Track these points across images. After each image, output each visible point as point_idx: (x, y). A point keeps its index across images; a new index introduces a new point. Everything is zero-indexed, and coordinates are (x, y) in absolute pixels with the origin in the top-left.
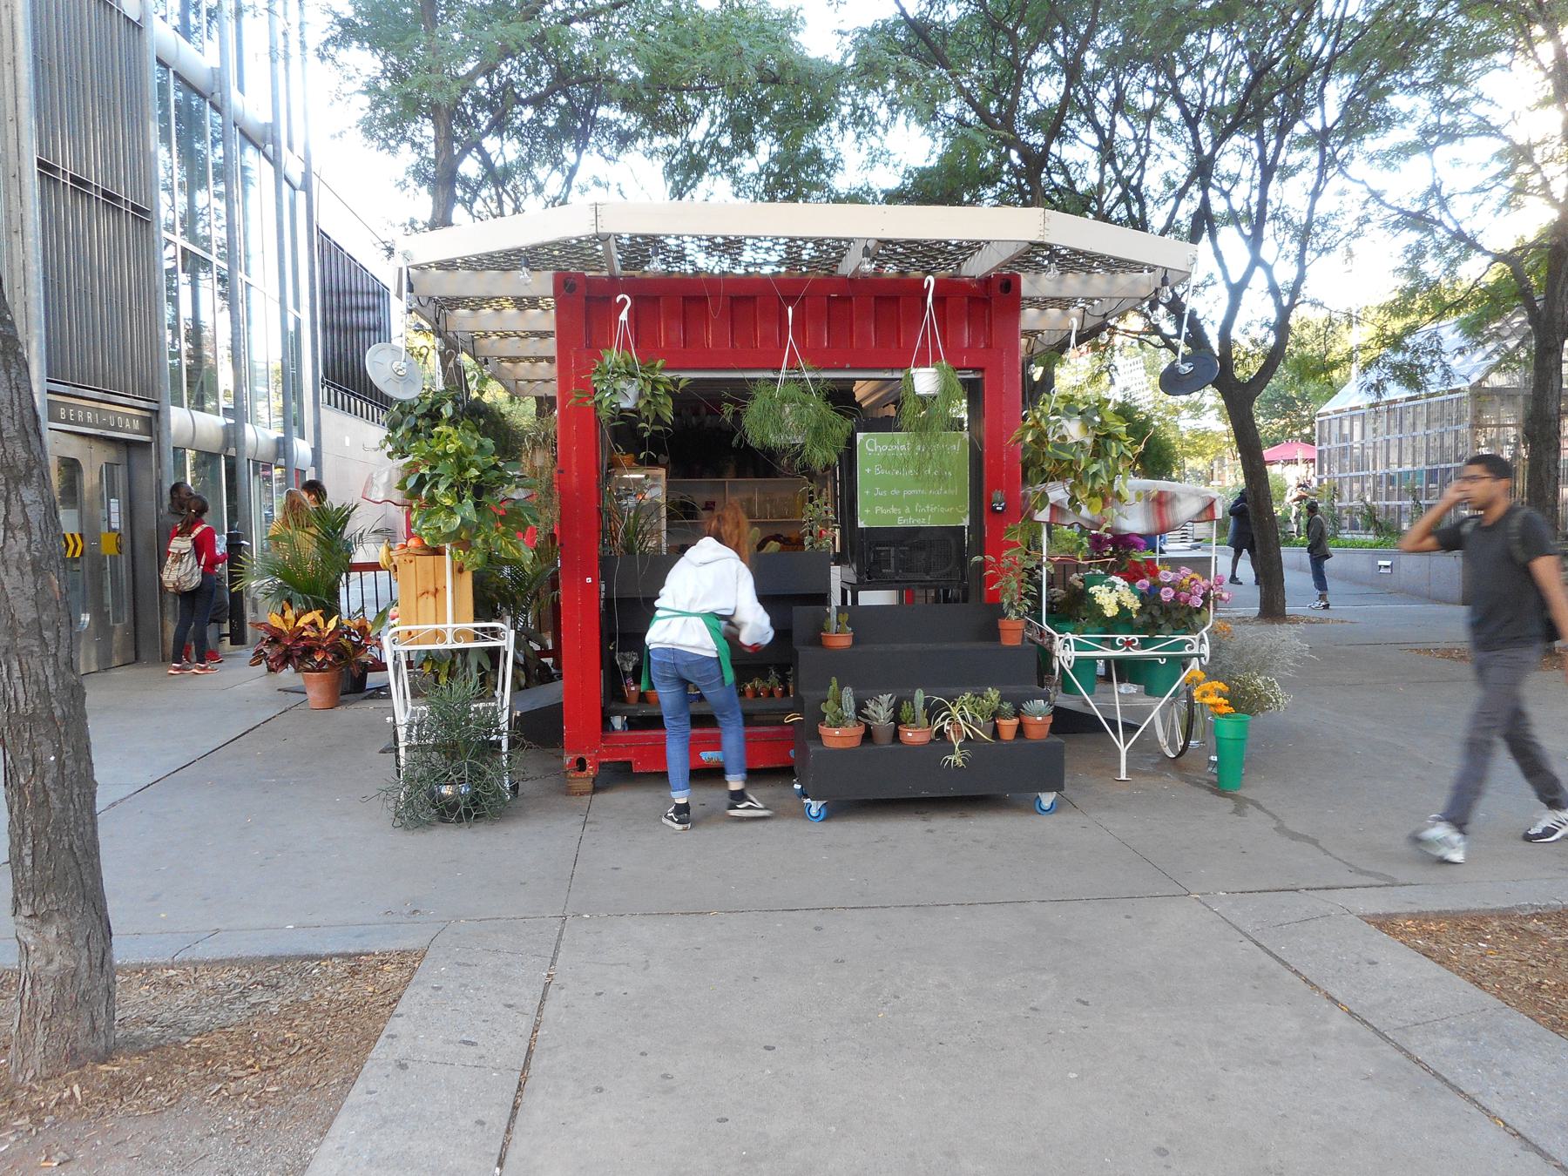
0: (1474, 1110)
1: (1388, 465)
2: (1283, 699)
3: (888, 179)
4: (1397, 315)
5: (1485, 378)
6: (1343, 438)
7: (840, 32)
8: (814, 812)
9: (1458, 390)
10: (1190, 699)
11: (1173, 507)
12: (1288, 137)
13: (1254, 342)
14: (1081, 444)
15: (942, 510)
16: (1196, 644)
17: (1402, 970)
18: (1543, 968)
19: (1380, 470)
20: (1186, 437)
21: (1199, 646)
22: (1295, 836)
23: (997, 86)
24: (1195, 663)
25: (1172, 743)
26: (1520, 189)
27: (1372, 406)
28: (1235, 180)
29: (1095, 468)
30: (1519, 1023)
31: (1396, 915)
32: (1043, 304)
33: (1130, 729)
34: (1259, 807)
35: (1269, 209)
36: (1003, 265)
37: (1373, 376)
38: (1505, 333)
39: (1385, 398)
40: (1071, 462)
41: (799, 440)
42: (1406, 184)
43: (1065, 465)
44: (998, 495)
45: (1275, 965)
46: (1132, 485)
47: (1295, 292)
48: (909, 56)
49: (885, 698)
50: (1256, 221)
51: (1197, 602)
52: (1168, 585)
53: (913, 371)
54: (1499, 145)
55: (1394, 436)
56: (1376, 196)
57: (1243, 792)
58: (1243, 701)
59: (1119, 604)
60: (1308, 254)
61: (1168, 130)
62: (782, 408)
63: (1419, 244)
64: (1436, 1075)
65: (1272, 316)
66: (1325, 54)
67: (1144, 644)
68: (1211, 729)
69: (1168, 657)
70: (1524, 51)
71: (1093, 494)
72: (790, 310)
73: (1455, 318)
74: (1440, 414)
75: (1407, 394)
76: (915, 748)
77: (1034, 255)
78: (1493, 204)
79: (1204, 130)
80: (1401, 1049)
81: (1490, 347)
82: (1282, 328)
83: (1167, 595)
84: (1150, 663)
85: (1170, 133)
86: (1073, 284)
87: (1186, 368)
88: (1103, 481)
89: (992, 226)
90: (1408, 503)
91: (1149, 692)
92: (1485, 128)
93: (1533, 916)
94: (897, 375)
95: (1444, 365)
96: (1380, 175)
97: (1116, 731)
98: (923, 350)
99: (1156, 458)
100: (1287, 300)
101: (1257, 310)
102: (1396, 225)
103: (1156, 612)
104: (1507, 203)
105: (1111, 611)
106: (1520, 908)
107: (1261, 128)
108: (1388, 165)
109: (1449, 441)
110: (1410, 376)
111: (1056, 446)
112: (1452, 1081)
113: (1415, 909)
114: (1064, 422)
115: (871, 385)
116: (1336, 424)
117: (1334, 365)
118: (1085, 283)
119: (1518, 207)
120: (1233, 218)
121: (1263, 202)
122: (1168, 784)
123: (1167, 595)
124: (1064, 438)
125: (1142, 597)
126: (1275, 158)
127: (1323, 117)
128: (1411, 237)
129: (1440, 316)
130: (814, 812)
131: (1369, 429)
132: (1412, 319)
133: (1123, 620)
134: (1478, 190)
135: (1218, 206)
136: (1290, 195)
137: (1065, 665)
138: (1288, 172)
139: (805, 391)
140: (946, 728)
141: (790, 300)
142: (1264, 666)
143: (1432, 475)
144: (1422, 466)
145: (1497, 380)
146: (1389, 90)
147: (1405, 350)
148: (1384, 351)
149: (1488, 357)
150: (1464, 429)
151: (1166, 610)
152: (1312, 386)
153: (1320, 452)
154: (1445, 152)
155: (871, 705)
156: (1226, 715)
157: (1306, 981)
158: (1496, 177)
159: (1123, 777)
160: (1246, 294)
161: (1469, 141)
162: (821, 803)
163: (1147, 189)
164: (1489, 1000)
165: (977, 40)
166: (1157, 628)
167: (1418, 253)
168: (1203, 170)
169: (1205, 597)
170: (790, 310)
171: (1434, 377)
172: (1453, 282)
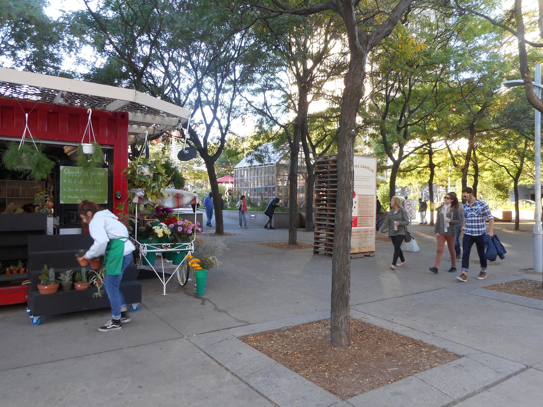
0: (267, 401)
1: (254, 185)
2: (218, 263)
3: (85, 70)
4: (256, 140)
5: (280, 161)
6: (241, 176)
7: (62, 11)
8: (35, 321)
9: (272, 164)
10: (188, 265)
11: (182, 199)
12: (225, 80)
13: (215, 144)
14: (149, 176)
15: (97, 197)
16: (190, 246)
17: (249, 353)
18: (289, 347)
19: (252, 187)
20: (196, 172)
21: (191, 247)
22: (220, 311)
23: (127, 44)
24: (189, 252)
25: (182, 280)
26: (288, 107)
27: (250, 167)
28: (209, 91)
29: (153, 185)
30: (281, 368)
31: (248, 335)
32: (139, 124)
33: (167, 275)
34: (210, 301)
35: (219, 102)
36: (119, 109)
37: (249, 158)
38: (285, 148)
39: (253, 165)
40: (145, 182)
41: (29, 168)
42: (258, 100)
43: (143, 183)
44: (118, 193)
45: (210, 359)
46: (171, 190)
47: (227, 129)
48: (88, 24)
49: (69, 272)
50: (216, 104)
51: (190, 232)
52: (181, 226)
53: (82, 144)
54: (283, 93)
55: (256, 177)
56: (250, 103)
57: (204, 296)
58: (205, 265)
59: (163, 232)
60: (231, 118)
61: (188, 70)
62: (21, 155)
63: (262, 119)
64: (257, 391)
65: (220, 136)
66: (236, 56)
67: (172, 247)
68: (195, 275)
69: (180, 251)
70: (289, 67)
71: (153, 194)
72: (27, 115)
73: (272, 143)
74: (268, 171)
75: (259, 164)
76: (81, 292)
77: (134, 106)
78: (281, 110)
79: (199, 73)
80: (247, 383)
81: (281, 152)
82: (222, 140)
83: (180, 229)
84: (174, 253)
85: (189, 73)
86: (149, 118)
87: (186, 152)
88: (156, 190)
89: (121, 94)
90: (260, 197)
91: (174, 263)
92: (280, 88)
93: (287, 330)
94: (77, 145)
95: (269, 156)
96: (250, 96)
97: (162, 277)
98: (87, 137)
99: (178, 181)
100: (224, 130)
101: (215, 133)
102: (255, 113)
103: (176, 235)
104: (285, 110)
105: (160, 235)
106: (283, 328)
107: (217, 77)
108: (254, 94)
109: (270, 179)
110: (260, 158)
111: (139, 175)
112: (261, 392)
113: (254, 332)
114: (143, 167)
115: (69, 148)
116: (239, 172)
117: (239, 153)
118: (153, 118)
119: (288, 112)
120: (208, 103)
121: (217, 99)
122: (181, 296)
123: (180, 229)
124: (142, 173)
125: (171, 230)
126: (221, 85)
127: (235, 76)
128: (259, 117)
129: (268, 141)
130: (35, 321)
131: (249, 173)
132: (261, 141)
133: (165, 238)
134: (277, 105)
135: (204, 98)
136: (225, 98)
137: (143, 255)
138: (225, 91)
139: (33, 148)
140: (95, 282)
141: (27, 111)
142: (212, 253)
143: (266, 189)
144: (263, 186)
145: (283, 162)
146: (254, 71)
147: (258, 150)
148: (252, 150)
149: (280, 155)
150: (274, 175)
151: (180, 234)
152: (234, 159)
153: (235, 180)
154: (268, 93)
155: (62, 275)
156: (200, 270)
157: (219, 364)
158: (282, 102)
159: (165, 294)
160: (212, 128)
161: (276, 91)
162: (38, 318)
163: (181, 89)
164: (273, 361)
165: (120, 26)
166: (177, 241)
167: (261, 122)
168: (198, 85)
169: (193, 230)
170: (27, 115)
171: (266, 159)
172: (271, 131)
